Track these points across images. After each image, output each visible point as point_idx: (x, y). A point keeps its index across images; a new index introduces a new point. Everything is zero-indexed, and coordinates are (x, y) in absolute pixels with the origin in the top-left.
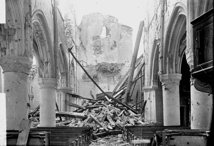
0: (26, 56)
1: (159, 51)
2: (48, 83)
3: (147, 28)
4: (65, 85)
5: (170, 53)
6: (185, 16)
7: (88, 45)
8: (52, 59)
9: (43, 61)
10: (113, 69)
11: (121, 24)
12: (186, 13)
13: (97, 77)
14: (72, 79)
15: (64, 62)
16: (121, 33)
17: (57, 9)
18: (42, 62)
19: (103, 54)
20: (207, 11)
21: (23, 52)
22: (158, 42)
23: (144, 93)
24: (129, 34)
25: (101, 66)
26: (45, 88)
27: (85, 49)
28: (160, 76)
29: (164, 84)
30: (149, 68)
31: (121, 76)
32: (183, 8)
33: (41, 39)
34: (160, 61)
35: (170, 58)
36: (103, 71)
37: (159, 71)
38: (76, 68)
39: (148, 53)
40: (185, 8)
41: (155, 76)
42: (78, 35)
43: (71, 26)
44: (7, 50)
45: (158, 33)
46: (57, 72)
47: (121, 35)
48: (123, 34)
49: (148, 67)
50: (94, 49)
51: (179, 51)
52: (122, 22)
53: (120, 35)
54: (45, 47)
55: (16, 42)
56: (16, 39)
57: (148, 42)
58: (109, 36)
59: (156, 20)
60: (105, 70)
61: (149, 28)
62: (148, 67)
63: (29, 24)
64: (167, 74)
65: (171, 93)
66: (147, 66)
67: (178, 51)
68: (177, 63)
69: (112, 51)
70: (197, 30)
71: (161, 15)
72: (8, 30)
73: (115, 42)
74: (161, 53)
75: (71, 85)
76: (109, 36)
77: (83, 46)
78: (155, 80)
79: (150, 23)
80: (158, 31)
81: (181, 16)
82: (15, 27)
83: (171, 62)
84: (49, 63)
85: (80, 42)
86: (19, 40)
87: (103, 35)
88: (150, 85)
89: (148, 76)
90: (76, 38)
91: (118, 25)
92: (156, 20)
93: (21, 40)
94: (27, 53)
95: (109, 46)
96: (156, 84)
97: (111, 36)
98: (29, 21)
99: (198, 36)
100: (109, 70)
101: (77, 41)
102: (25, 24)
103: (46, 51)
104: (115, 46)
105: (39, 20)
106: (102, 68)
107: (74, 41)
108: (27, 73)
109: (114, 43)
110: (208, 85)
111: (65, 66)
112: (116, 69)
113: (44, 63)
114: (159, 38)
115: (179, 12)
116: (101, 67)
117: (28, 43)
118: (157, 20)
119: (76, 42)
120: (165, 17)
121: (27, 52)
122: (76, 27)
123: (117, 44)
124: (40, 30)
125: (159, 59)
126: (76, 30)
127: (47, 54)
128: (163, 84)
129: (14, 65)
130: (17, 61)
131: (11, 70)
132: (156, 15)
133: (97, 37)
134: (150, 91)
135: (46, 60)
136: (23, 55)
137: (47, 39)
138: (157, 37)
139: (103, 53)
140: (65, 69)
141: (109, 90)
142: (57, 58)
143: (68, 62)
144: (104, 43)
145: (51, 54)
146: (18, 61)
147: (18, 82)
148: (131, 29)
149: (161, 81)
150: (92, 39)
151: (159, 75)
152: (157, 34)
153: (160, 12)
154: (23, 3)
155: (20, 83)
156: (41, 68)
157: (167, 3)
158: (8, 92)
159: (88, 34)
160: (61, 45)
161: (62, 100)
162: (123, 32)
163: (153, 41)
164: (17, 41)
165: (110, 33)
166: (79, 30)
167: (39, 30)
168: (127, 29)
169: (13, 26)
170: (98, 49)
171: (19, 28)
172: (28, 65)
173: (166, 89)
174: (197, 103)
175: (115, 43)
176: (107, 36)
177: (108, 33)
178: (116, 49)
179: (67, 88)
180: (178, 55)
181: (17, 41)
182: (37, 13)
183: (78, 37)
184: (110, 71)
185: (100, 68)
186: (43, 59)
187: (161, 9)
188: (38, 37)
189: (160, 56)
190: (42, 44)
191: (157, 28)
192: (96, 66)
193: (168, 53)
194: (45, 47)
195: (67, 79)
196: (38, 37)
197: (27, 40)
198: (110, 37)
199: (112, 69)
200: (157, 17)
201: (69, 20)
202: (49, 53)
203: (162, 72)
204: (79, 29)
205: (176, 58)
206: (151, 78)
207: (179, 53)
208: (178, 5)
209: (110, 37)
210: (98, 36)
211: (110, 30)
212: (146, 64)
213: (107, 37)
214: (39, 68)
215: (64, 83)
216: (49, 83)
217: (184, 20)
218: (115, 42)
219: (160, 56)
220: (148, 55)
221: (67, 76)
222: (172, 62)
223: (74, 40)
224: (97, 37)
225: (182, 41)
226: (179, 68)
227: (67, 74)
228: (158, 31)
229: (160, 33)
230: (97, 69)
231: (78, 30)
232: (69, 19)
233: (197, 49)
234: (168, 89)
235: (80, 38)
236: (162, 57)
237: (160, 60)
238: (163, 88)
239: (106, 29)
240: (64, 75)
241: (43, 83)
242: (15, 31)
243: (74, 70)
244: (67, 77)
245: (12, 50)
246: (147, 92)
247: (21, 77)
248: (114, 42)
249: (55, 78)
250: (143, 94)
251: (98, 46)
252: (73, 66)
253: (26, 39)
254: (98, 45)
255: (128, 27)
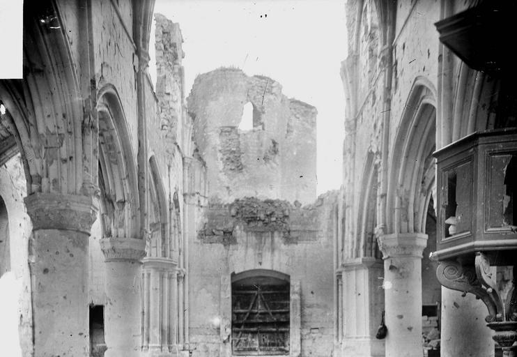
0: (85, 195)
1: (379, 181)
2: (123, 250)
3: (353, 122)
4: (160, 251)
5: (402, 186)
6: (434, 108)
7: (209, 149)
8: (133, 193)
9: (113, 199)
10: (271, 214)
11: (289, 98)
12: (435, 100)
13: (233, 233)
14: (175, 239)
15: (158, 198)
16: (290, 120)
17: (145, 76)
18: (111, 202)
19: (245, 173)
20: (459, 138)
21: (80, 185)
22: (376, 158)
23: (344, 275)
24: (310, 122)
25: (242, 207)
26: (115, 260)
27: (204, 164)
28: (380, 239)
29: (389, 257)
30: (356, 217)
31: (289, 232)
32: (429, 90)
33: (110, 149)
34: (379, 205)
35: (401, 198)
36: (247, 218)
37: (378, 227)
38: (184, 211)
39: (354, 179)
40: (432, 91)
41: (369, 234)
42: (188, 130)
43: (171, 108)
44: (44, 181)
45: (377, 137)
46: (144, 226)
47: (290, 124)
48: (295, 122)
49: (353, 213)
50: (222, 159)
51: (423, 182)
52: (290, 92)
53: (288, 124)
54: (119, 168)
55: (63, 163)
56: (65, 156)
57: (354, 154)
58: (260, 127)
59: (373, 106)
60: (253, 216)
61: (358, 122)
62: (353, 213)
63: (91, 124)
64: (395, 235)
65: (403, 277)
66: (350, 211)
67: (421, 181)
68: (417, 210)
69: (268, 165)
70: (444, 171)
71: (385, 98)
72: (45, 136)
73: (274, 143)
74: (381, 187)
75: (173, 253)
76: (260, 127)
77: (200, 159)
78: (369, 245)
79: (359, 110)
80: (377, 134)
81: (427, 106)
82: (63, 131)
83: (404, 206)
84: (126, 203)
85: (194, 148)
86: (71, 158)
87: (245, 124)
88: (357, 256)
89: (353, 234)
90: (183, 139)
91: (282, 101)
92: (373, 106)
93: (74, 159)
94: (88, 189)
95: (260, 151)
96: (370, 254)
97: (266, 128)
98: (91, 117)
99: (445, 185)
100: (262, 216)
101: (186, 145)
102: (83, 122)
103: (120, 175)
104: (276, 152)
105: (107, 106)
106: (245, 210)
107: (178, 147)
108: (87, 231)
109: (272, 145)
110: (462, 277)
111: (160, 207)
112: (279, 213)
113: (115, 204)
114: (379, 148)
115: (422, 99)
116: (244, 209)
117: (89, 165)
118: (375, 106)
119: (183, 146)
120: (392, 102)
121: (87, 186)
122: (183, 111)
123: (279, 147)
124: (108, 128)
125: (378, 199)
126: (183, 118)
127: (122, 184)
128: (387, 257)
129: (59, 213)
130: (67, 206)
131: (52, 225)
132: (372, 95)
133: (230, 129)
134: (356, 270)
135: (119, 198)
136: (78, 192)
137: (124, 148)
138: (375, 146)
139: (243, 170)
140: (161, 215)
141: (260, 263)
142: (144, 192)
143: (167, 197)
144: (246, 144)
145: (131, 183)
146: (68, 207)
147: (68, 251)
148: (313, 110)
149: (380, 249)
150: (218, 134)
151: (377, 236)
152: (374, 139)
153: (383, 90)
154: (79, 75)
155: (72, 255)
156: (107, 214)
157: (396, 71)
158: (46, 275)
159: (208, 121)
160: (151, 160)
161: (151, 288)
162: (293, 118)
163: (365, 154)
164: (65, 161)
165: (264, 118)
166: (190, 118)
167: (106, 129)
168: (303, 109)
169: (58, 128)
170: (235, 162)
171: (69, 131)
172: (89, 214)
173: (392, 268)
174: (455, 304)
175: (274, 146)
176: (254, 126)
177: (257, 115)
178: (277, 159)
179: (164, 258)
180: (420, 190)
181: (65, 161)
182: (103, 93)
183: (188, 135)
184: (263, 219)
185: (240, 211)
186: (114, 194)
187: (383, 84)
188: (102, 143)
189: (380, 191)
190: (112, 160)
191: (375, 126)
192: (231, 206)
193: (399, 186)
194: (119, 168)
195: (164, 239)
196: (102, 143)
197: (88, 158)
198: (263, 129)
199: (268, 215)
200: (374, 98)
201: (169, 94)
202: (127, 181)
203: (384, 229)
204: (191, 116)
205: (415, 199)
206: (359, 240)
207: (422, 186)
208: (419, 82)
209: (263, 129)
210: (233, 128)
211: (264, 113)
212: (348, 206)
213: (256, 129)
214: (103, 215)
215: (156, 247)
216: (127, 249)
217: (431, 121)
218: (274, 143)
219: (380, 191)
220: (353, 184)
221: (164, 231)
222: (407, 207)
223: (179, 144)
224: (230, 129)
225: (429, 159)
226: (422, 222)
227: (164, 225)
228: (377, 134)
229: (380, 138)
230: (234, 214)
231: (188, 120)
232: (167, 92)
233: (443, 206)
234: (396, 268)
235: (192, 138)
236: (384, 196)
237: (380, 201)
238: (386, 265)
239: (252, 109)
240: (157, 230)
241: (114, 250)
242: (62, 139)
243: (178, 215)
244: (164, 232)
245: (55, 181)
246: (349, 271)
247: (74, 242)
248: (271, 142)
249: (141, 238)
250: (341, 276)
251: (234, 152)
252: (177, 207)
253: (85, 158)
254: (233, 149)
255: (307, 106)
